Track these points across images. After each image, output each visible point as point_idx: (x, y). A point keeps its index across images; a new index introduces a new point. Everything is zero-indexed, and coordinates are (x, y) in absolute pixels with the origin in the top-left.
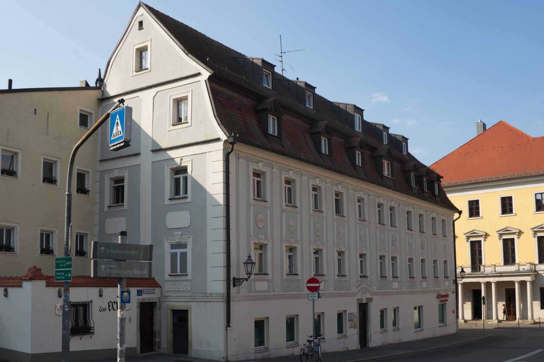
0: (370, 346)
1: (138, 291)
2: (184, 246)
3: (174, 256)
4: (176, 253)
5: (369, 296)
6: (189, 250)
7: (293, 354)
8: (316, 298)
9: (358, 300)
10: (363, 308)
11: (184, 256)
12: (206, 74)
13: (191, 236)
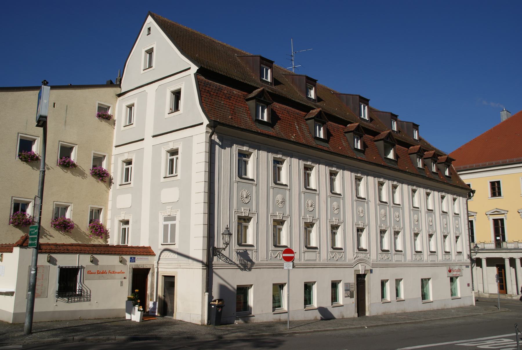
0: (139, 321)
1: (131, 258)
2: (174, 219)
3: (166, 227)
4: (168, 225)
5: (368, 268)
6: (177, 222)
7: (280, 319)
8: (291, 268)
9: (355, 271)
10: (360, 279)
11: (173, 226)
12: (195, 68)
13: (179, 210)
